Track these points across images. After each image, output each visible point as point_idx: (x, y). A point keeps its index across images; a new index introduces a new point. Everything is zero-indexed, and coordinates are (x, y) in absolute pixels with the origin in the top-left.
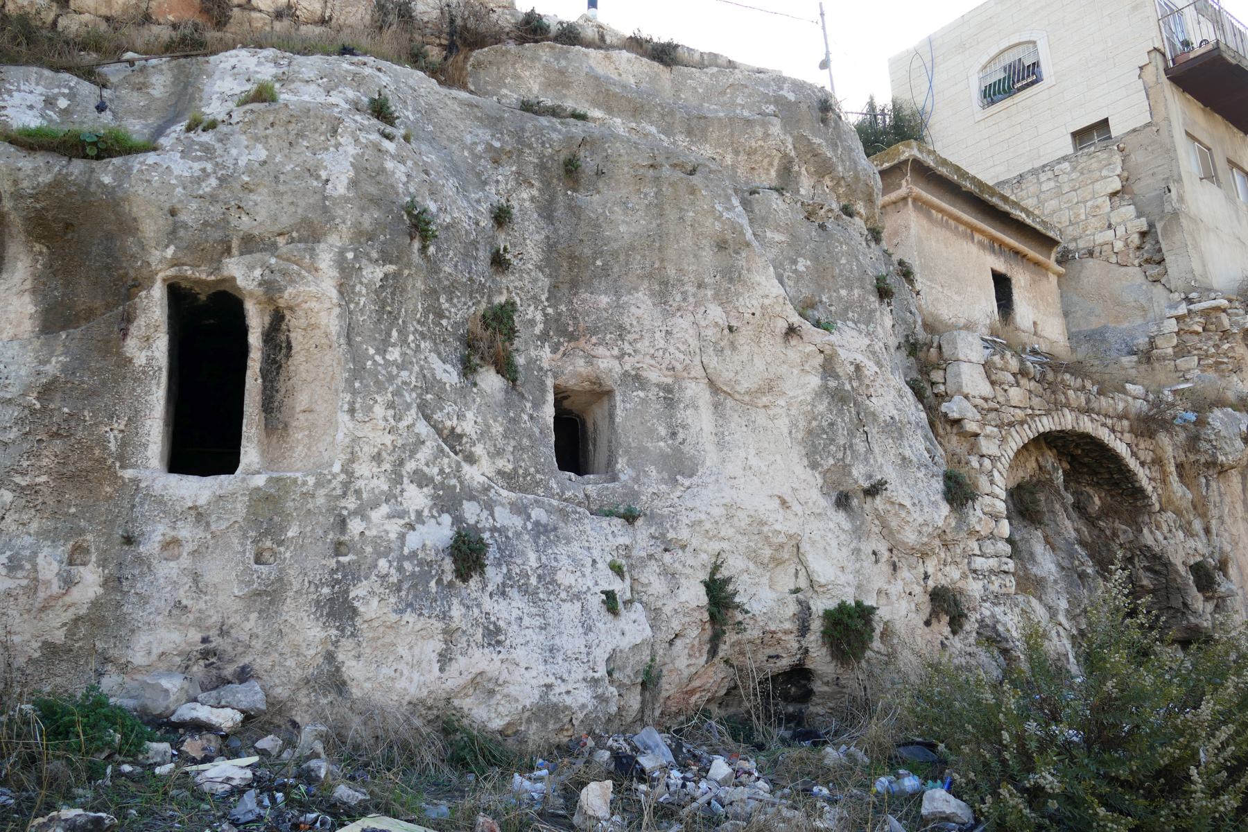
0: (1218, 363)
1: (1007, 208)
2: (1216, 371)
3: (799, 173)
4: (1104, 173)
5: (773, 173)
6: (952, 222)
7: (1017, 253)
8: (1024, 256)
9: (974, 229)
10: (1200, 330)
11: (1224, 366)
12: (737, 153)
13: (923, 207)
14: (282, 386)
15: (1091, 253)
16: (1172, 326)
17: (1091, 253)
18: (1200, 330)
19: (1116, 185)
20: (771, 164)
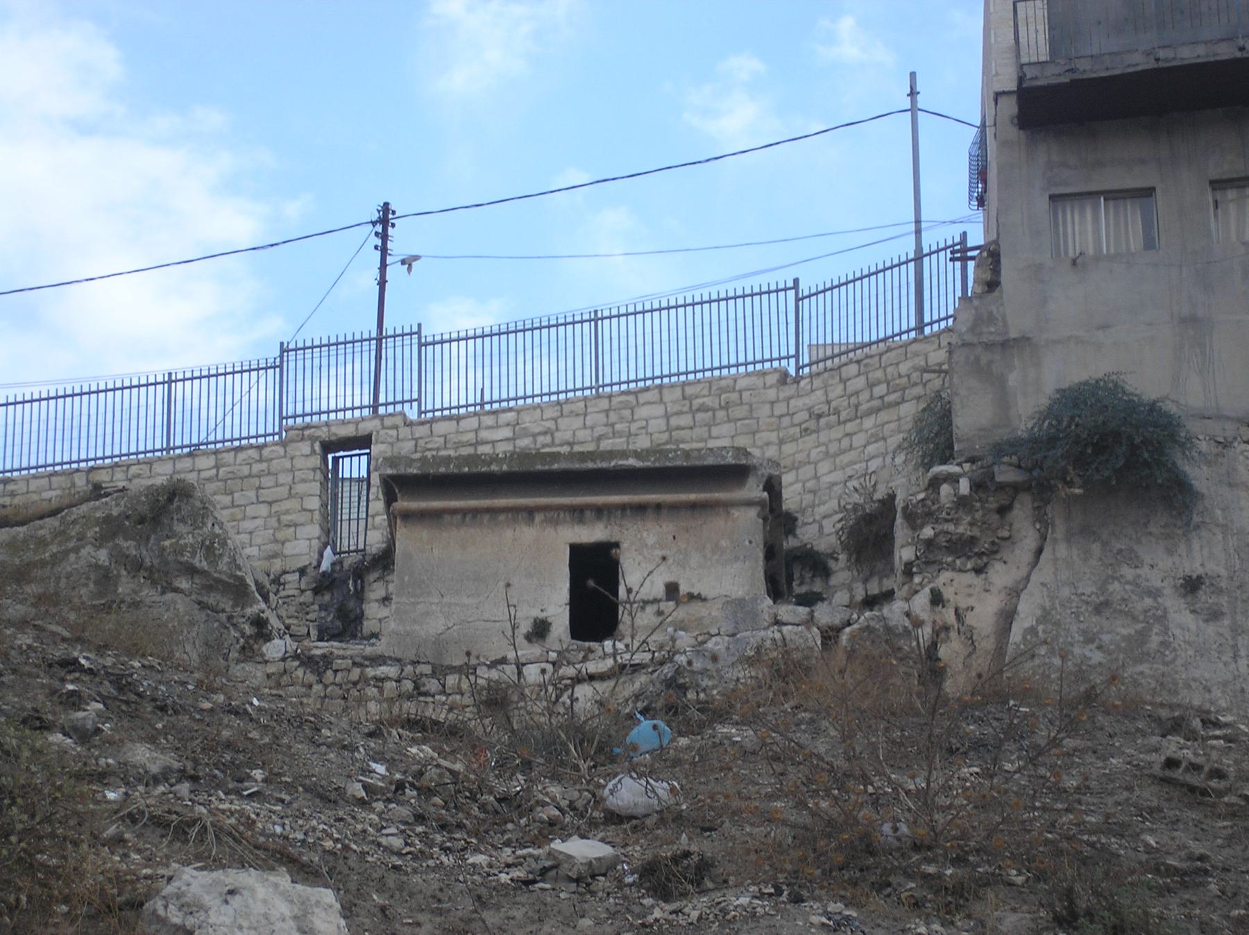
3: (119, 576)
7: (693, 506)
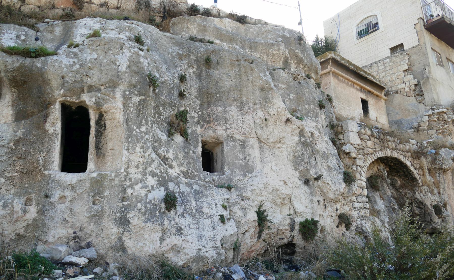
0: (443, 132)
1: (366, 76)
2: (442, 135)
3: (291, 63)
4: (402, 63)
5: (281, 63)
6: (346, 81)
8: (373, 93)
9: (354, 83)
10: (437, 120)
11: (445, 133)
12: (268, 56)
13: (336, 75)
14: (103, 140)
15: (397, 92)
16: (426, 118)
17: (397, 92)
18: (437, 120)
19: (406, 67)
20: (280, 60)
